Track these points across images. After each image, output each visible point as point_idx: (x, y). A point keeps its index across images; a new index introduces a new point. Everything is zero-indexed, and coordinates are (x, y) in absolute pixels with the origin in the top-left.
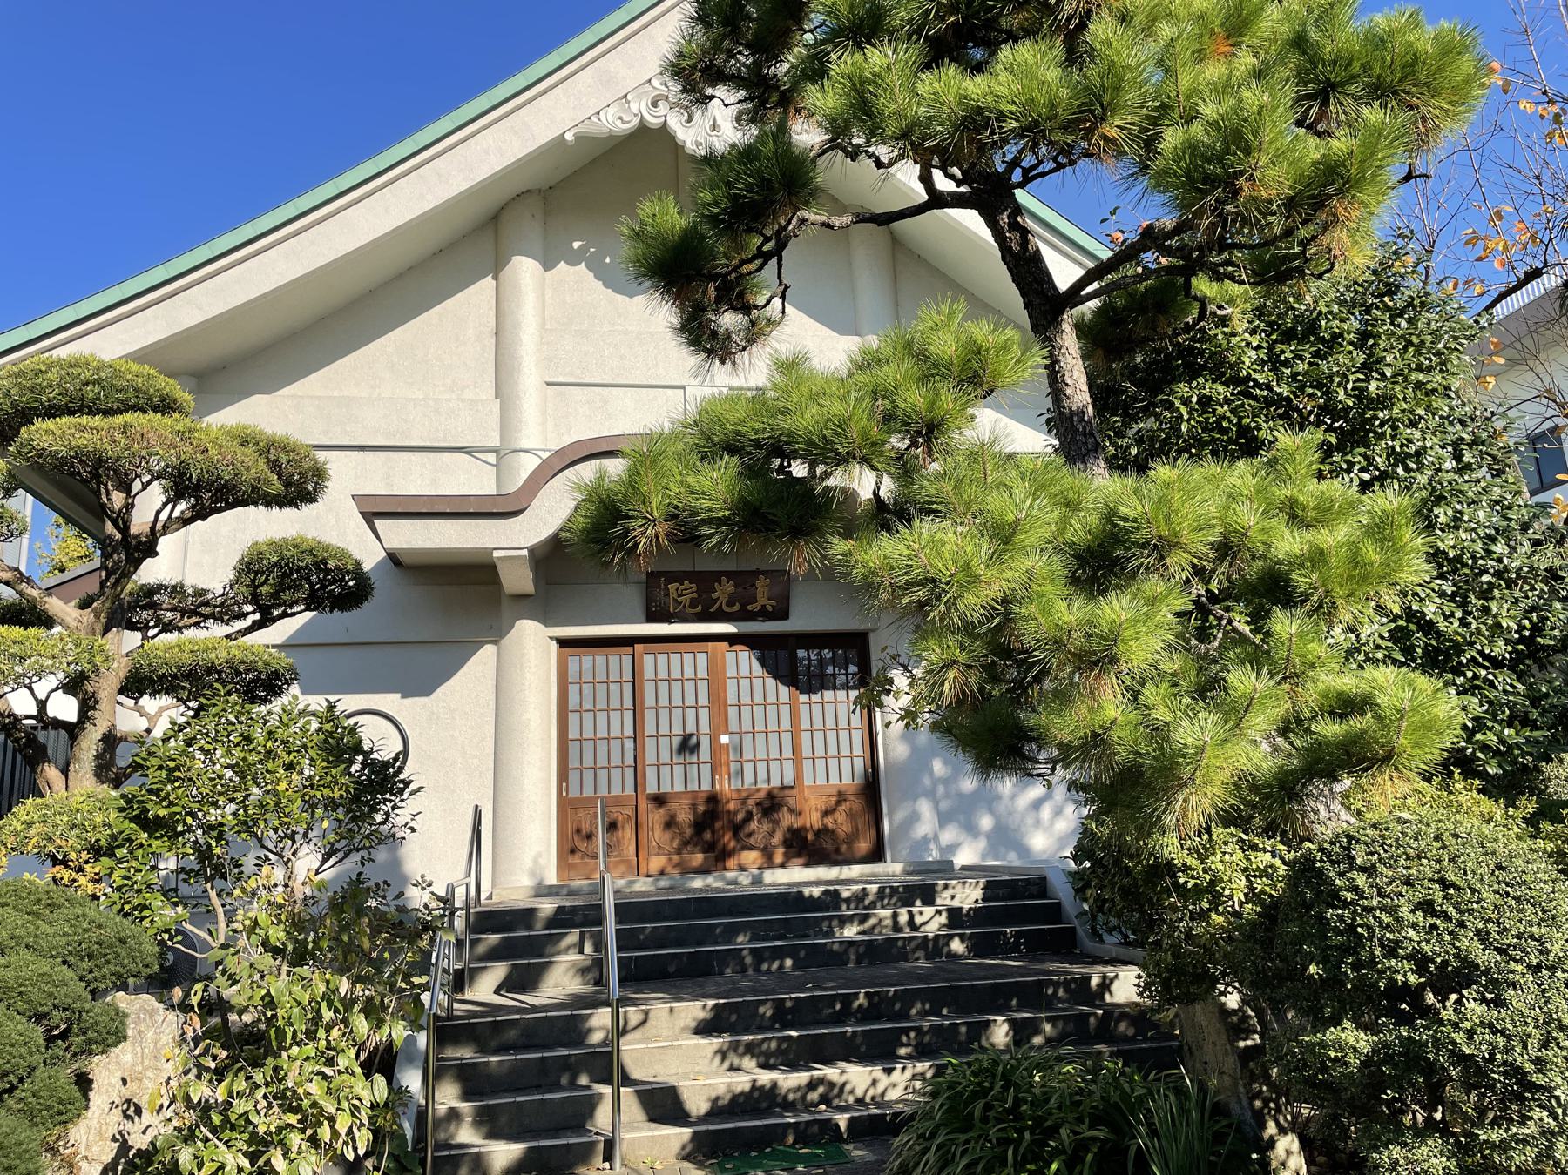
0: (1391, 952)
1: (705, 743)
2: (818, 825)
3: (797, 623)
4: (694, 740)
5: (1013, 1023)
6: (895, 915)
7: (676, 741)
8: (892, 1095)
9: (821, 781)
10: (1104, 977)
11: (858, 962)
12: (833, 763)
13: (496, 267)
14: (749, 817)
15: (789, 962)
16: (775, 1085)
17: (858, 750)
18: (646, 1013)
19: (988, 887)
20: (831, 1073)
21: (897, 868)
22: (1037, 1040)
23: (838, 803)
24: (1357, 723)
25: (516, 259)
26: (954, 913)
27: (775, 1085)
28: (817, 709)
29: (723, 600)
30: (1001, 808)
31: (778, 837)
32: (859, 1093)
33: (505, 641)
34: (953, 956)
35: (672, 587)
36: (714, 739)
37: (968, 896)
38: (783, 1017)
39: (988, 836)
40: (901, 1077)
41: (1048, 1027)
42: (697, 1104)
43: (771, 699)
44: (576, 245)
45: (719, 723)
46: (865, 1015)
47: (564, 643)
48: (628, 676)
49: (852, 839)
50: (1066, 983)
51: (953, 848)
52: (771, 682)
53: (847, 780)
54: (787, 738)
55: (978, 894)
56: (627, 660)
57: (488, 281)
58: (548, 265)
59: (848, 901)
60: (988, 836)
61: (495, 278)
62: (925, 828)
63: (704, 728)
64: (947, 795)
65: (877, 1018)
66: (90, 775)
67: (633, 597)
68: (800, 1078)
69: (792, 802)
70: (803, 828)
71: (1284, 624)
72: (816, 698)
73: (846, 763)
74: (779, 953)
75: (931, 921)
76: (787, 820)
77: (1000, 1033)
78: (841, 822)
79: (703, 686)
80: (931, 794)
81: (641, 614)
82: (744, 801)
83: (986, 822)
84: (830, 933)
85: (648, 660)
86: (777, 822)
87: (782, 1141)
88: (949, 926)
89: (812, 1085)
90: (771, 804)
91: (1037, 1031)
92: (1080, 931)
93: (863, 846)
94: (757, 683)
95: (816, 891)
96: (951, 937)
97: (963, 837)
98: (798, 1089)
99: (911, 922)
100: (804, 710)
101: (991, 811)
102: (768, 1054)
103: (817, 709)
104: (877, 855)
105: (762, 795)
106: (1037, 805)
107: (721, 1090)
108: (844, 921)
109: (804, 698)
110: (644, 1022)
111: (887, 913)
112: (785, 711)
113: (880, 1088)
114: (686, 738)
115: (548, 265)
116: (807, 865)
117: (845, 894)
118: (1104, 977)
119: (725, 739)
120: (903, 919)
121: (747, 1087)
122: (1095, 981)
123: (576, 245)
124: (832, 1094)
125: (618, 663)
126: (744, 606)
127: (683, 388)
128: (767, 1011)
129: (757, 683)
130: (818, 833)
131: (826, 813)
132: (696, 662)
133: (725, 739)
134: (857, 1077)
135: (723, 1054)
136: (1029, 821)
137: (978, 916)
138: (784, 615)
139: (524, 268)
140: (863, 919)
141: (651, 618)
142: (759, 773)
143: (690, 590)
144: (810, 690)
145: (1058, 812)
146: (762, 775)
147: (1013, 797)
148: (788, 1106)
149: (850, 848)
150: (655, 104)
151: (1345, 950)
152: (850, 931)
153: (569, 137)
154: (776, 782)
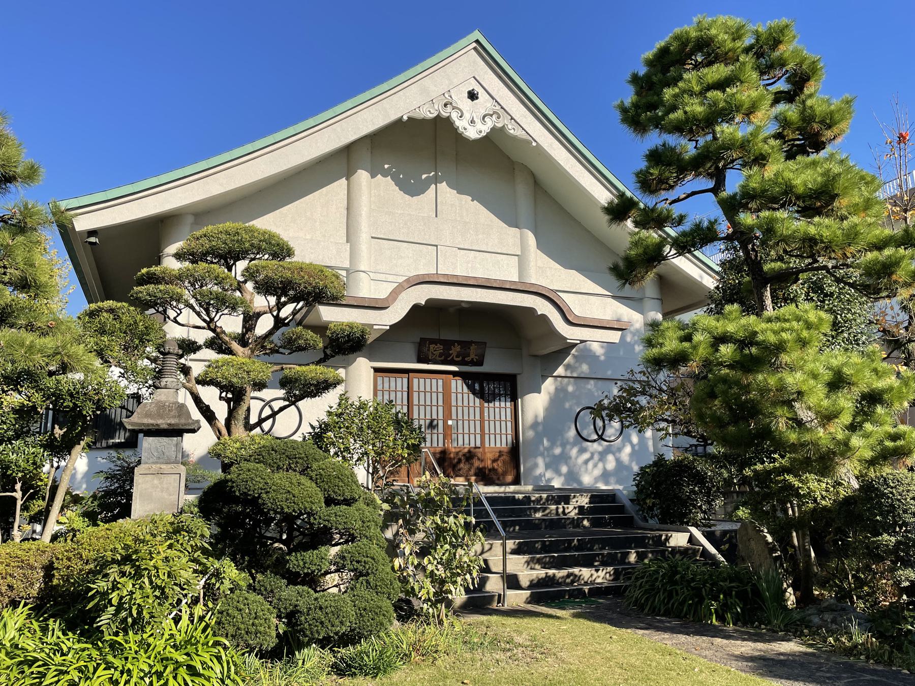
0: (905, 511)
1: (441, 423)
2: (490, 467)
3: (486, 368)
4: (435, 422)
5: (637, 553)
6: (557, 508)
7: (428, 422)
8: (599, 580)
9: (493, 445)
10: (667, 535)
11: (546, 528)
12: (498, 437)
13: (349, 174)
14: (460, 461)
15: (517, 528)
16: (554, 575)
17: (509, 431)
18: (492, 545)
19: (592, 497)
20: (576, 570)
21: (530, 488)
22: (646, 561)
23: (500, 456)
24: (900, 443)
25: (359, 171)
26: (581, 508)
27: (554, 575)
28: (492, 410)
29: (455, 354)
30: (571, 462)
31: (472, 472)
32: (586, 579)
33: (352, 368)
34: (584, 527)
35: (432, 346)
36: (445, 423)
37: (584, 501)
38: (546, 548)
39: (565, 475)
40: (601, 573)
41: (650, 555)
42: (525, 582)
43: (471, 404)
44: (386, 166)
45: (448, 415)
46: (577, 549)
47: (377, 370)
48: (405, 389)
49: (505, 474)
50: (653, 538)
51: (549, 480)
52: (471, 396)
53: (504, 445)
54: (478, 423)
55: (587, 500)
56: (405, 380)
57: (343, 181)
58: (373, 176)
59: (533, 501)
60: (565, 475)
61: (347, 179)
62: (540, 469)
63: (441, 417)
64: (548, 456)
65: (582, 550)
66: (242, 427)
67: (411, 350)
68: (563, 573)
69: (479, 455)
70: (484, 468)
71: (879, 410)
72: (491, 405)
73: (504, 437)
74: (513, 523)
75: (571, 511)
76: (477, 463)
77: (633, 558)
78: (499, 466)
79: (440, 395)
80: (542, 455)
81: (415, 358)
82: (457, 453)
83: (564, 469)
84: (530, 515)
85: (415, 381)
86: (472, 464)
87: (564, 597)
88: (579, 514)
89: (569, 576)
90: (470, 456)
91: (646, 557)
92: (636, 517)
93: (509, 478)
94: (466, 396)
95: (521, 496)
96: (583, 519)
97: (554, 475)
98: (563, 577)
99: (564, 512)
100: (486, 410)
101: (567, 464)
102: (545, 563)
103: (492, 410)
104: (516, 481)
105: (466, 450)
106: (586, 462)
107: (534, 577)
108: (536, 510)
109: (486, 405)
110: (490, 549)
111: (554, 507)
112: (478, 410)
113: (594, 577)
114: (432, 421)
115: (373, 176)
116: (485, 485)
117: (533, 499)
118: (667, 535)
119: (450, 422)
120: (560, 510)
121: (544, 576)
122: (663, 538)
123: (386, 166)
124: (577, 578)
125: (401, 382)
126: (464, 358)
127: (436, 246)
128: (539, 546)
129: (466, 396)
130: (490, 470)
131: (494, 461)
132: (437, 383)
133: (450, 422)
134: (585, 573)
135: (528, 563)
136: (583, 469)
137: (591, 511)
138: (480, 363)
139: (362, 176)
140: (544, 509)
141: (420, 361)
142: (463, 441)
143: (439, 348)
144: (488, 402)
145: (595, 466)
146: (467, 441)
147: (577, 458)
148: (559, 584)
149: (504, 478)
150: (445, 105)
151: (889, 512)
152: (539, 515)
153: (405, 118)
154: (472, 445)
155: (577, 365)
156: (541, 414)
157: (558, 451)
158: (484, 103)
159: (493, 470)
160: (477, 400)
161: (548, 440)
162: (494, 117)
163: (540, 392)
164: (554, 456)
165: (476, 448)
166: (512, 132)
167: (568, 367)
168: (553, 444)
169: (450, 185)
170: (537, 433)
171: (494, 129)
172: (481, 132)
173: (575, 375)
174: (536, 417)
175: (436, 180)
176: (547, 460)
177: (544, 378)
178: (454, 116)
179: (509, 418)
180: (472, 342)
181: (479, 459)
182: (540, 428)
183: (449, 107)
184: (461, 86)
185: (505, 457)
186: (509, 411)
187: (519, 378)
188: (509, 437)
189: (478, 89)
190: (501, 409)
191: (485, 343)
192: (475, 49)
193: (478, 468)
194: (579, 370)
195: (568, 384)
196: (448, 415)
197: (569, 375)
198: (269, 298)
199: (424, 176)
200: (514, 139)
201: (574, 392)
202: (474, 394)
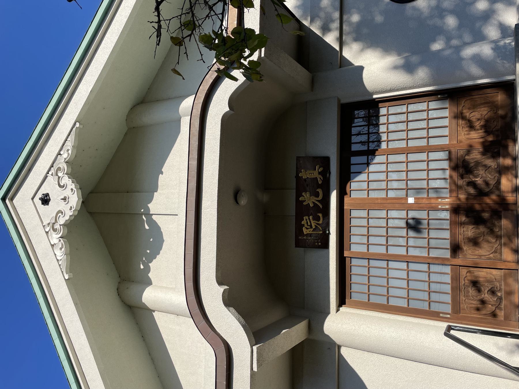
1: (412, 214)
3: (332, 151)
7: (411, 233)
23: (463, 118)
29: (314, 199)
31: (490, 162)
33: (338, 341)
44: (142, 267)
47: (342, 302)
49: (493, 106)
51: (503, 28)
52: (372, 168)
57: (155, 314)
58: (149, 283)
61: (154, 311)
62: (486, 50)
63: (403, 214)
67: (313, 256)
70: (483, 144)
72: (384, 137)
76: (476, 155)
78: (478, 115)
80: (458, 49)
81: (322, 252)
86: (478, 164)
90: (461, 166)
100: (392, 145)
103: (392, 136)
105: (455, 175)
109: (384, 146)
112: (392, 158)
114: (409, 226)
115: (149, 283)
126: (319, 186)
129: (372, 177)
131: (471, 127)
132: (357, 218)
133: (411, 200)
138: (325, 161)
141: (326, 245)
155: (322, 14)
156: (391, 59)
157: (451, 21)
158: (50, 187)
159: (487, 128)
160: (378, 159)
161: (434, 40)
162: (60, 174)
163: (361, 68)
164: (460, 26)
165: (450, 159)
166: (70, 152)
167: (326, 29)
168: (438, 31)
169: (150, 201)
170: (422, 63)
171: (71, 175)
172: (72, 190)
173: (337, 15)
174: (396, 68)
175: (149, 215)
176: (467, 38)
177: (344, 63)
178: (62, 221)
179: (404, 109)
180: (297, 177)
181: (468, 152)
182: (415, 59)
183: (57, 226)
184: (43, 209)
185: (464, 106)
186: (392, 110)
187: (344, 101)
188: (433, 105)
189: (39, 195)
190: (390, 119)
191: (298, 158)
192: (12, 199)
193: (484, 153)
194: (330, 10)
195: (350, 24)
196: (400, 204)
197: (336, 24)
198: (381, 114)
199: (147, 227)
200: (78, 148)
201: (360, 11)
202: (368, 164)
